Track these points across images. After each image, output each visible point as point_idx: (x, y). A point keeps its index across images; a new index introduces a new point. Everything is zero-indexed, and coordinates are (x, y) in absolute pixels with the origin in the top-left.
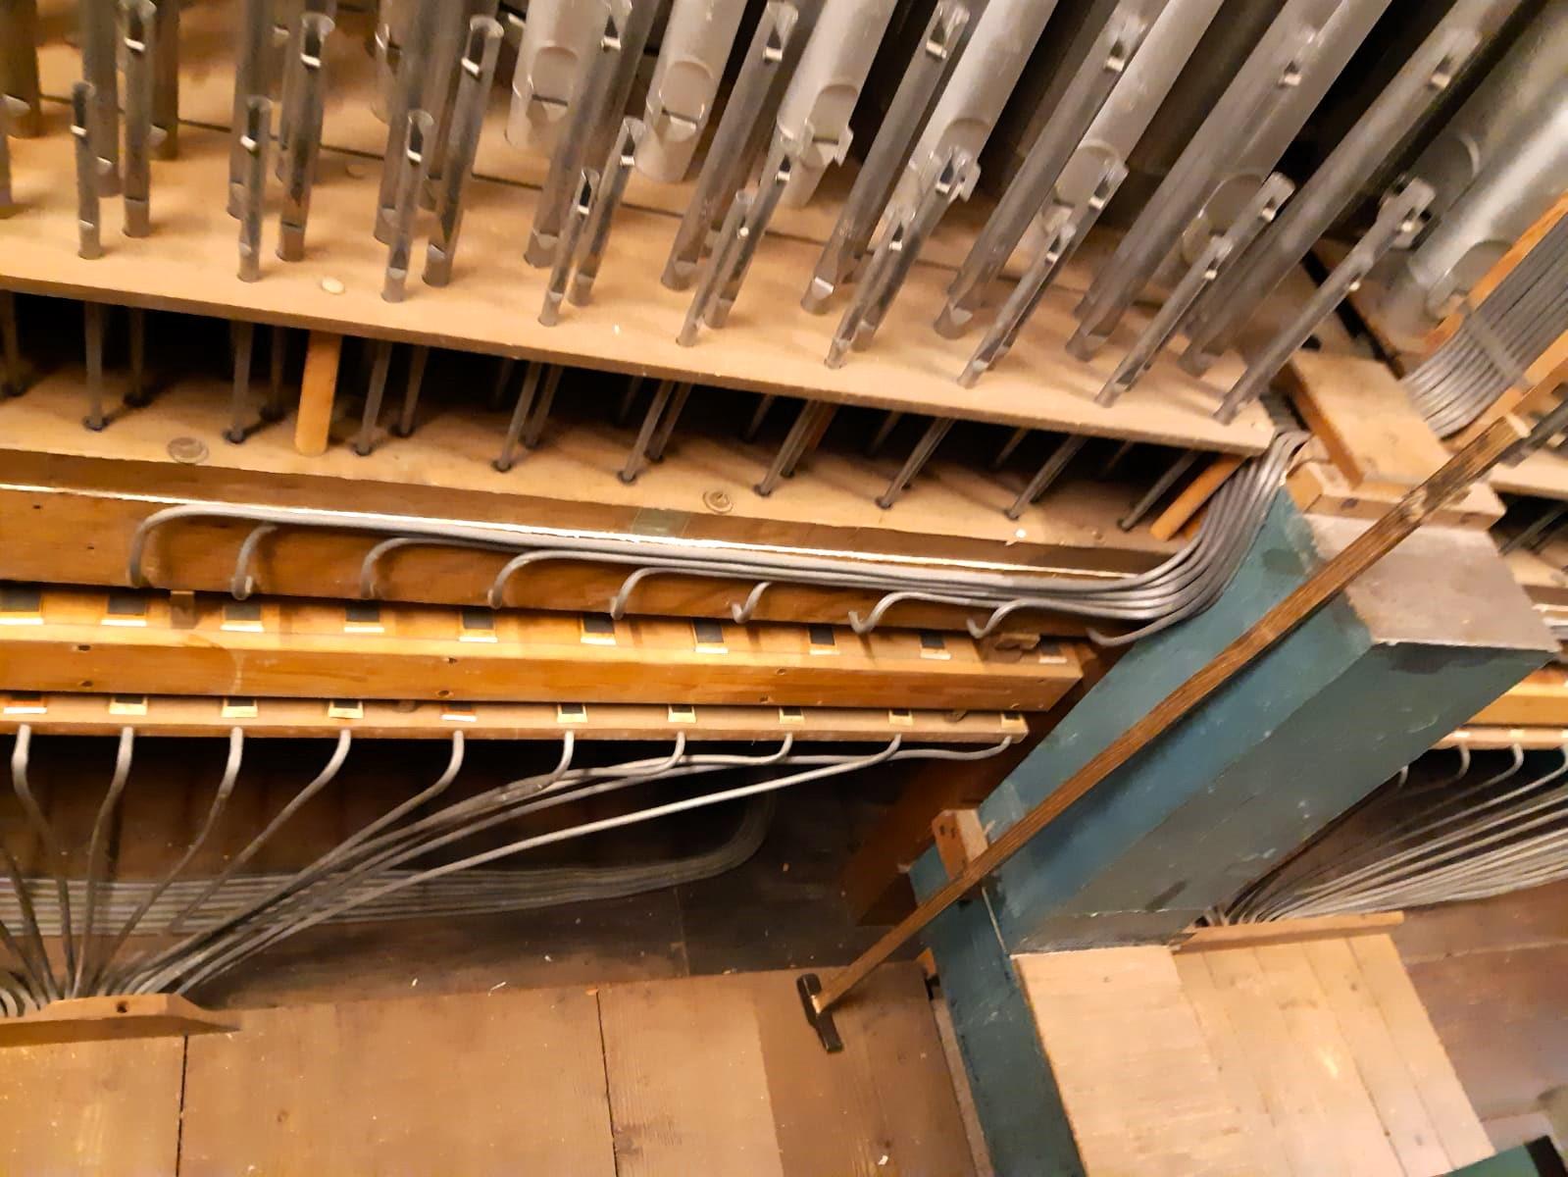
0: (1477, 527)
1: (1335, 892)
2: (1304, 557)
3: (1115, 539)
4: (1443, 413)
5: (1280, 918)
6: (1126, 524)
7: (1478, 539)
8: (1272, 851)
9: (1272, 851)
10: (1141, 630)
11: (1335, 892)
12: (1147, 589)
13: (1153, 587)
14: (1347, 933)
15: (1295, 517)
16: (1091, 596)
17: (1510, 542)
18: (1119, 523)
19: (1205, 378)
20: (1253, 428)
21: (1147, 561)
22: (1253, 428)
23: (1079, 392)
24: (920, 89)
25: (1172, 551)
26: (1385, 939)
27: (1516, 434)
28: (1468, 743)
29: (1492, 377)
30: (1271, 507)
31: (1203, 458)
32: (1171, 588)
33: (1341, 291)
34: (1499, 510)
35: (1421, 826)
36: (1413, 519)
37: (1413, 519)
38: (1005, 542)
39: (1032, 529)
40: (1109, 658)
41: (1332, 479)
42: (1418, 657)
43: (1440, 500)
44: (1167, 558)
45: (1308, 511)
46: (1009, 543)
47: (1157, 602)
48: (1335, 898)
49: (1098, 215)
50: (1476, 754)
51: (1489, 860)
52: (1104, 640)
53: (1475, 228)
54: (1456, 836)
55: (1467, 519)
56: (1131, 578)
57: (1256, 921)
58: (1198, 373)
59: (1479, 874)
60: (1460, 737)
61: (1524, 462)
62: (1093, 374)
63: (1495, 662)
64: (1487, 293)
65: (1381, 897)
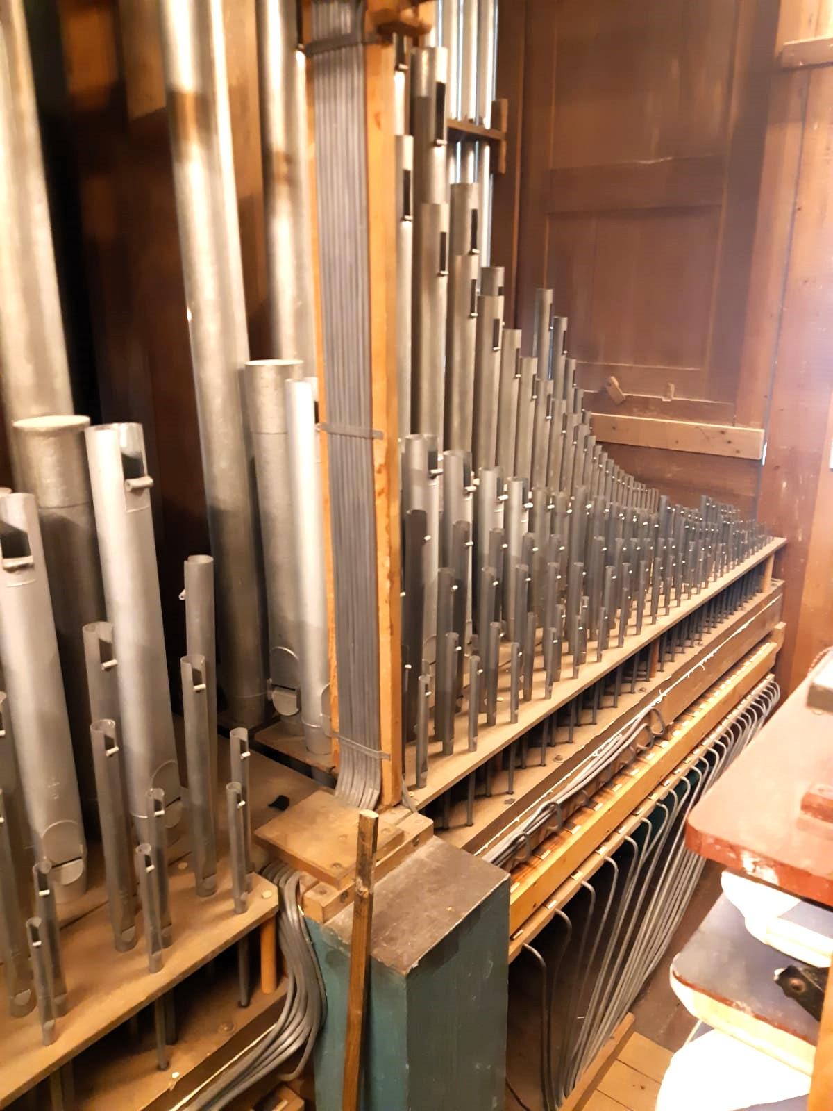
0: (427, 838)
1: (587, 1039)
2: (341, 949)
3: (243, 1018)
4: (363, 800)
5: (576, 1083)
6: (244, 1003)
7: (435, 841)
8: (495, 1099)
9: (495, 1099)
10: (305, 1053)
11: (587, 1039)
12: (286, 1029)
13: (288, 1027)
14: (613, 1057)
15: (321, 929)
16: (256, 1064)
17: (486, 784)
18: (240, 1006)
19: (219, 891)
20: (265, 897)
21: (272, 1013)
22: (265, 897)
23: (137, 975)
24: (486, 32)
25: (283, 994)
26: (636, 1038)
27: (371, 819)
28: (557, 907)
29: (371, 761)
30: (308, 931)
31: (252, 937)
32: (299, 1015)
33: (237, 810)
34: (430, 822)
35: (590, 952)
36: (366, 896)
37: (366, 896)
38: (169, 1089)
39: (183, 1063)
40: (309, 1074)
41: (323, 892)
42: (437, 956)
43: (369, 877)
44: (284, 998)
45: (325, 921)
46: (171, 1089)
47: (299, 1029)
48: (592, 1042)
49: (205, 691)
50: (537, 942)
51: (641, 939)
52: (290, 1077)
53: (316, 689)
54: (613, 941)
55: (416, 842)
56: (275, 1028)
57: (566, 1098)
58: (212, 891)
59: (645, 950)
60: (513, 949)
61: (427, 781)
62: (140, 953)
63: (483, 913)
64: (338, 721)
65: (609, 1023)
